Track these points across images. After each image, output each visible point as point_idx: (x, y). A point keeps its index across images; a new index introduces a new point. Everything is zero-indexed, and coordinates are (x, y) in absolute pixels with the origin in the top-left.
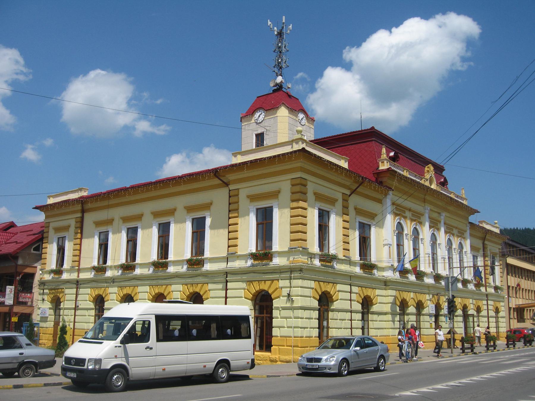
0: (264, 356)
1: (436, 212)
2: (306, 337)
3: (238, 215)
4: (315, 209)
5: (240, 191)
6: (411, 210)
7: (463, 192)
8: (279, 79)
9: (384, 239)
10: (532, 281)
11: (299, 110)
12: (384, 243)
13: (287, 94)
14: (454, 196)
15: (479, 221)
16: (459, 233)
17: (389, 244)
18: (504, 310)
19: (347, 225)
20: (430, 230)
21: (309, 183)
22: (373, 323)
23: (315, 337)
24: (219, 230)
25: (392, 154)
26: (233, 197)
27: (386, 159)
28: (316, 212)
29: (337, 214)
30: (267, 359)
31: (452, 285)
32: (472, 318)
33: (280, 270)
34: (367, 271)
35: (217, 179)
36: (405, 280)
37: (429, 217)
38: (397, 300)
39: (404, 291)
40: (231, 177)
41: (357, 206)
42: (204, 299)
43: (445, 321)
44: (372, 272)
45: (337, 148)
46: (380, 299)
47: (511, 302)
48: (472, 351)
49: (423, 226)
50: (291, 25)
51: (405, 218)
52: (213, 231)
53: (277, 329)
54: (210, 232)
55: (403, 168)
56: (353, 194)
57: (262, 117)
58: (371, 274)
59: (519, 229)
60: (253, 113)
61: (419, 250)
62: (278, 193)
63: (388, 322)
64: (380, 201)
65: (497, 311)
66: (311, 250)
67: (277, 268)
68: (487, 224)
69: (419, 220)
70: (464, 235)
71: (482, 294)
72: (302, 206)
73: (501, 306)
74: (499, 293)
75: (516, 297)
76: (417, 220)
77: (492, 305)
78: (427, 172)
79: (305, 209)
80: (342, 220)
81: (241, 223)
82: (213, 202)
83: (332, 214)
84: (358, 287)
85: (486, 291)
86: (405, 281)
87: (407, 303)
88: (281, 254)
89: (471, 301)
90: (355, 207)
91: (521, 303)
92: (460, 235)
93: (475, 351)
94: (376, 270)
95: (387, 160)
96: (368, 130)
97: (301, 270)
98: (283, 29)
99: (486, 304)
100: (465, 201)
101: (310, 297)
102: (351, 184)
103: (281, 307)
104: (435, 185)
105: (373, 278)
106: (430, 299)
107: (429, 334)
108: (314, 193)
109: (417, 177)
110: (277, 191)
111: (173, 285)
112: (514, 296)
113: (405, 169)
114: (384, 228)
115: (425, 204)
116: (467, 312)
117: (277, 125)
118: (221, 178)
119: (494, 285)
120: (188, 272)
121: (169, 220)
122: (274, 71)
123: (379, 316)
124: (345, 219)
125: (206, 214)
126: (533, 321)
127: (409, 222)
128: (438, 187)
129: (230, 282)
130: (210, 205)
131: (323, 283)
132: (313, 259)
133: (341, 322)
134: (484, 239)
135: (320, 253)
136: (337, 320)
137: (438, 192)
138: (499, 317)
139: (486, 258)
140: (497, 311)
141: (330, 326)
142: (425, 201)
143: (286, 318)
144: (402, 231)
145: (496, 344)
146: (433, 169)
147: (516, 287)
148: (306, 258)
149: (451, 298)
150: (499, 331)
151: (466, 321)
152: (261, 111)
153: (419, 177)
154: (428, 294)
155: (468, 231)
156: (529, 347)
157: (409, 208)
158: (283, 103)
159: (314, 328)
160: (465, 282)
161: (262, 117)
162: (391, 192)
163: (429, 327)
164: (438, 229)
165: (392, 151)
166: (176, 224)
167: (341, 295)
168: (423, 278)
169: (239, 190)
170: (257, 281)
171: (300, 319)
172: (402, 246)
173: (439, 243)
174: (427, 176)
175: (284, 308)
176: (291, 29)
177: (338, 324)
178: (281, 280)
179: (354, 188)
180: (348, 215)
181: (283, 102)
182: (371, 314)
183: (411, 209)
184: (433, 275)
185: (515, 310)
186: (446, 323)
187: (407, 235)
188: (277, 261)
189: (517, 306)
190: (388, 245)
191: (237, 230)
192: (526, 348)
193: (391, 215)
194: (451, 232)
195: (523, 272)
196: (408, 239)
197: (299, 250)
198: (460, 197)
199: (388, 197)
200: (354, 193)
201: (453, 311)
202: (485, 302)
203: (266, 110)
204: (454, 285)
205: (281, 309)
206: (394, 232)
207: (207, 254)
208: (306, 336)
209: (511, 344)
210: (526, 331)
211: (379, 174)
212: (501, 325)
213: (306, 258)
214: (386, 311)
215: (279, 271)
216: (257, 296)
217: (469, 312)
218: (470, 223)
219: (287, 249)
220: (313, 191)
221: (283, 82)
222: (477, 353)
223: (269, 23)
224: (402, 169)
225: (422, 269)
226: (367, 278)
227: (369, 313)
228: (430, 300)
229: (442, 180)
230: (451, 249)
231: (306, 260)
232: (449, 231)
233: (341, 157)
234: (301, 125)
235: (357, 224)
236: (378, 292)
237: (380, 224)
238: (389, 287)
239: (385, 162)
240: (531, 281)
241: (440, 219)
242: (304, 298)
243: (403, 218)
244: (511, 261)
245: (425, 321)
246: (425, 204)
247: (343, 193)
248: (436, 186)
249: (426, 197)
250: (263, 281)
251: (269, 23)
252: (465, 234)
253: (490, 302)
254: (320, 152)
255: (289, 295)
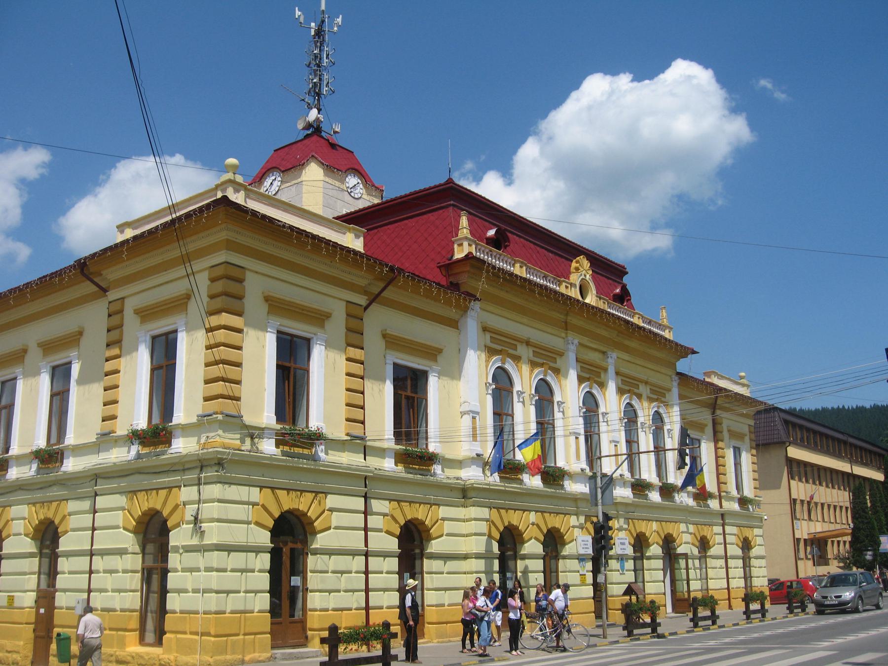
0: (149, 657)
1: (595, 350)
2: (232, 612)
3: (121, 351)
4: (267, 332)
5: (126, 300)
6: (531, 343)
7: (665, 314)
8: (313, 114)
9: (462, 400)
10: (829, 488)
11: (348, 169)
12: (463, 409)
13: (327, 142)
14: (641, 320)
15: (704, 373)
16: (653, 394)
17: (471, 411)
18: (763, 543)
19: (357, 369)
20: (579, 385)
21: (249, 276)
22: (432, 579)
23: (260, 612)
24: (91, 386)
25: (491, 233)
26: (116, 312)
27: (466, 238)
28: (270, 341)
29: (329, 345)
30: (156, 662)
31: (603, 493)
32: (684, 560)
33: (182, 465)
34: (417, 467)
35: (89, 282)
36: (513, 487)
37: (577, 358)
38: (493, 528)
39: (668, 521)
40: (112, 274)
41: (386, 330)
42: (61, 533)
43: (619, 568)
44: (429, 471)
45: (386, 227)
46: (448, 527)
47: (800, 528)
48: (654, 630)
49: (562, 378)
50: (341, 16)
51: (517, 359)
52: (82, 388)
53: (174, 596)
54: (78, 390)
55: (513, 259)
56: (373, 304)
57: (277, 184)
58: (646, 497)
59: (846, 407)
60: (261, 179)
61: (638, 444)
62: (186, 300)
63: (471, 575)
64: (454, 324)
65: (746, 545)
66: (249, 419)
67: (177, 461)
68: (722, 377)
69: (552, 365)
70: (665, 397)
71: (712, 513)
72: (226, 324)
73: (756, 536)
74: (751, 510)
75: (824, 521)
76: (548, 364)
77: (735, 535)
78: (574, 271)
79: (240, 331)
80: (344, 357)
81: (126, 367)
82: (84, 330)
83: (317, 344)
84: (388, 502)
85: (721, 506)
86: (512, 487)
87: (647, 540)
88: (187, 430)
89: (683, 527)
90: (384, 332)
91: (819, 529)
92: (655, 397)
93: (660, 630)
94: (440, 467)
95: (470, 240)
96: (440, 185)
97: (220, 463)
98: (324, 24)
99: (721, 532)
100: (667, 331)
101: (249, 523)
102: (369, 284)
103: (183, 547)
104: (594, 296)
105: (431, 483)
106: (581, 524)
107: (579, 596)
108: (264, 297)
109: (549, 278)
110: (184, 294)
111: (14, 505)
112: (806, 517)
113: (515, 262)
114: (462, 378)
115: (567, 333)
116: (676, 549)
117: (302, 198)
118: (95, 280)
119: (739, 496)
120: (39, 476)
121: (14, 373)
122: (303, 100)
123: (448, 562)
124: (352, 356)
125: (73, 354)
126: (839, 563)
127: (526, 368)
128: (602, 301)
129: (101, 495)
130: (78, 337)
131: (285, 492)
132: (256, 440)
133: (337, 576)
134: (713, 407)
135: (279, 427)
136: (351, 573)
137: (602, 311)
138: (753, 558)
139: (720, 443)
140: (746, 545)
141: (310, 586)
142: (566, 326)
143: (191, 570)
144: (594, 408)
145: (717, 614)
146: (589, 265)
147: (808, 502)
148: (238, 436)
149: (601, 520)
150: (753, 585)
151: (674, 566)
152: (275, 173)
153: (554, 278)
154: (576, 515)
155: (675, 391)
156: (798, 615)
157: (189, 240)
158: (313, 156)
159: (256, 592)
160: (667, 491)
161: (277, 184)
162: (476, 305)
163: (579, 582)
164: (602, 385)
165: (492, 226)
166: (26, 379)
167: (336, 519)
168: (563, 481)
169: (124, 301)
170: (143, 490)
171: (214, 573)
172: (511, 418)
173: (605, 411)
174: (575, 278)
175: (189, 549)
176: (340, 24)
177: (330, 580)
178: (184, 486)
179: (376, 290)
180: (362, 349)
181: (314, 154)
182: (427, 558)
183: (531, 340)
184: (587, 475)
185: (808, 543)
186: (621, 574)
187: (520, 393)
188: (181, 446)
189: (812, 536)
190: (469, 414)
191: (117, 384)
192: (792, 617)
193: (478, 353)
194: (633, 390)
195: (834, 476)
196: (523, 403)
197: (216, 420)
198: (656, 323)
199: (470, 313)
200: (377, 300)
201: (604, 547)
202: (718, 529)
203: (283, 172)
204: (607, 492)
205: (181, 551)
206: (487, 389)
207: (71, 439)
208: (231, 611)
209: (797, 607)
210: (811, 583)
211: (450, 266)
212: (755, 572)
213: (238, 436)
214: (465, 552)
215: (181, 468)
216: (148, 524)
217: (678, 549)
218: (679, 374)
219: (194, 420)
220: (263, 293)
221: (321, 120)
222: (666, 634)
223: (298, 13)
224: (509, 260)
225: (561, 463)
226: (389, 479)
227: (424, 556)
228: (581, 527)
229: (618, 291)
230: (662, 431)
231: (238, 442)
232: (627, 388)
233: (346, 227)
234: (351, 198)
235: (390, 370)
236: (443, 511)
237: (454, 372)
238: (471, 500)
239: (466, 244)
240: (839, 489)
241: (605, 363)
242: (229, 524)
243: (510, 358)
244: (794, 452)
245: (568, 570)
246: (567, 333)
247: (348, 302)
248: (595, 298)
249: (569, 318)
250: (155, 491)
251: (298, 13)
252: (667, 395)
253: (728, 529)
254: (322, 227)
255: (196, 520)
